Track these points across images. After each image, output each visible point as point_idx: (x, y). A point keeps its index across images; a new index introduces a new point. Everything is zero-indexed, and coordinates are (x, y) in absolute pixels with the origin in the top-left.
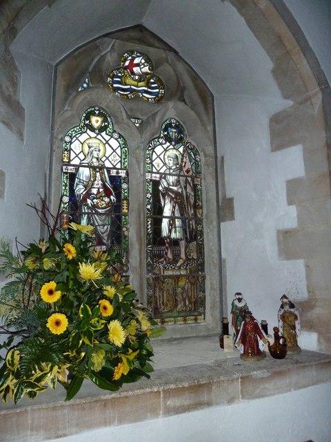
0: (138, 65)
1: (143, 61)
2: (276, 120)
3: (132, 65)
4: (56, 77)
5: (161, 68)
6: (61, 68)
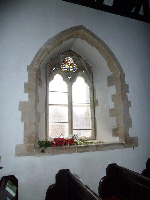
0: (70, 61)
1: (71, 60)
2: (109, 78)
3: (68, 61)
4: (47, 68)
5: (77, 61)
6: (48, 65)
